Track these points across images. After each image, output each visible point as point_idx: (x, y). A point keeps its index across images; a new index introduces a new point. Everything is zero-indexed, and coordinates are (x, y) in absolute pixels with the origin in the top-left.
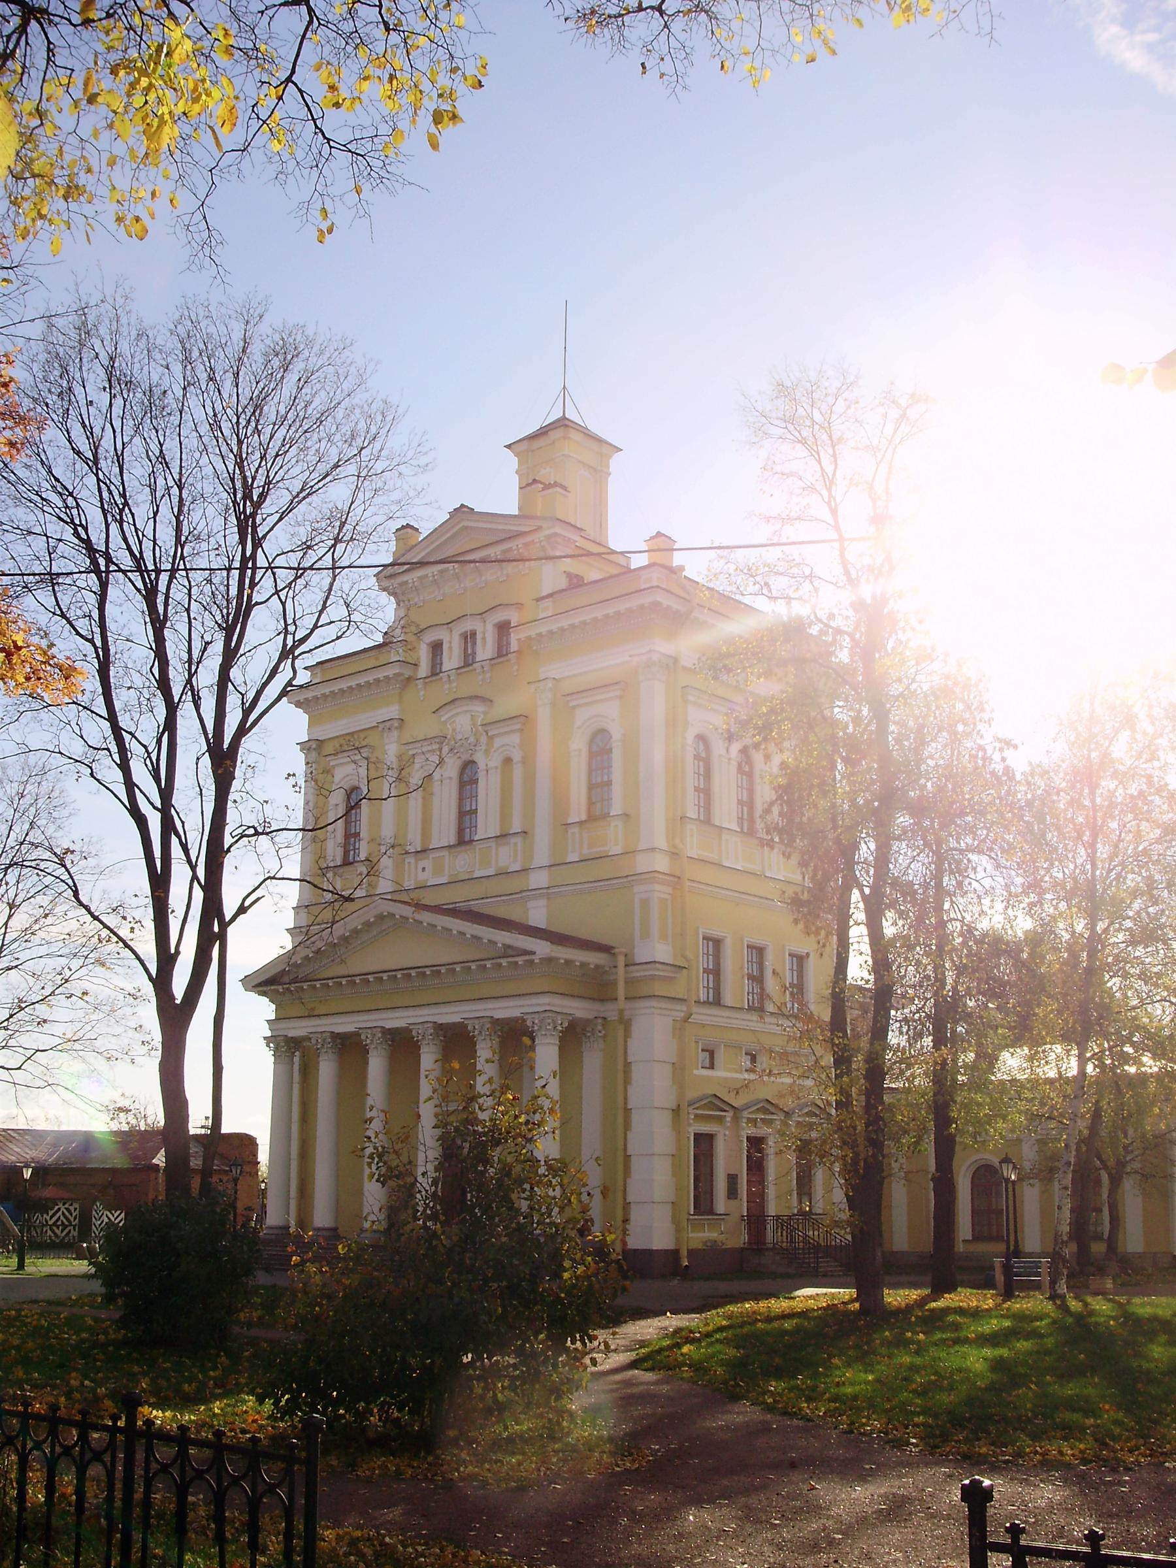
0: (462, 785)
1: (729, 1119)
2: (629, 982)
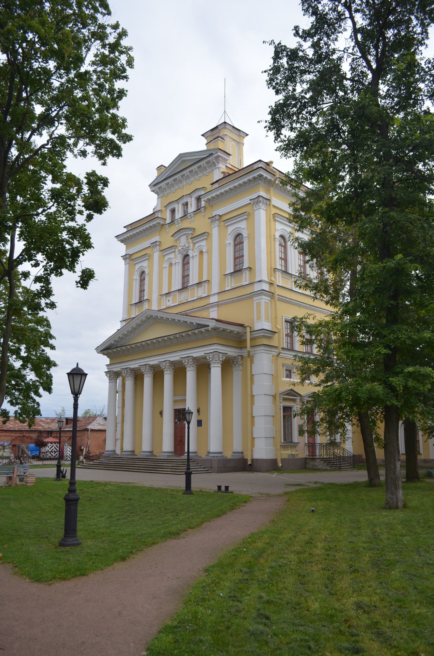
1: (298, 400)
2: (251, 339)
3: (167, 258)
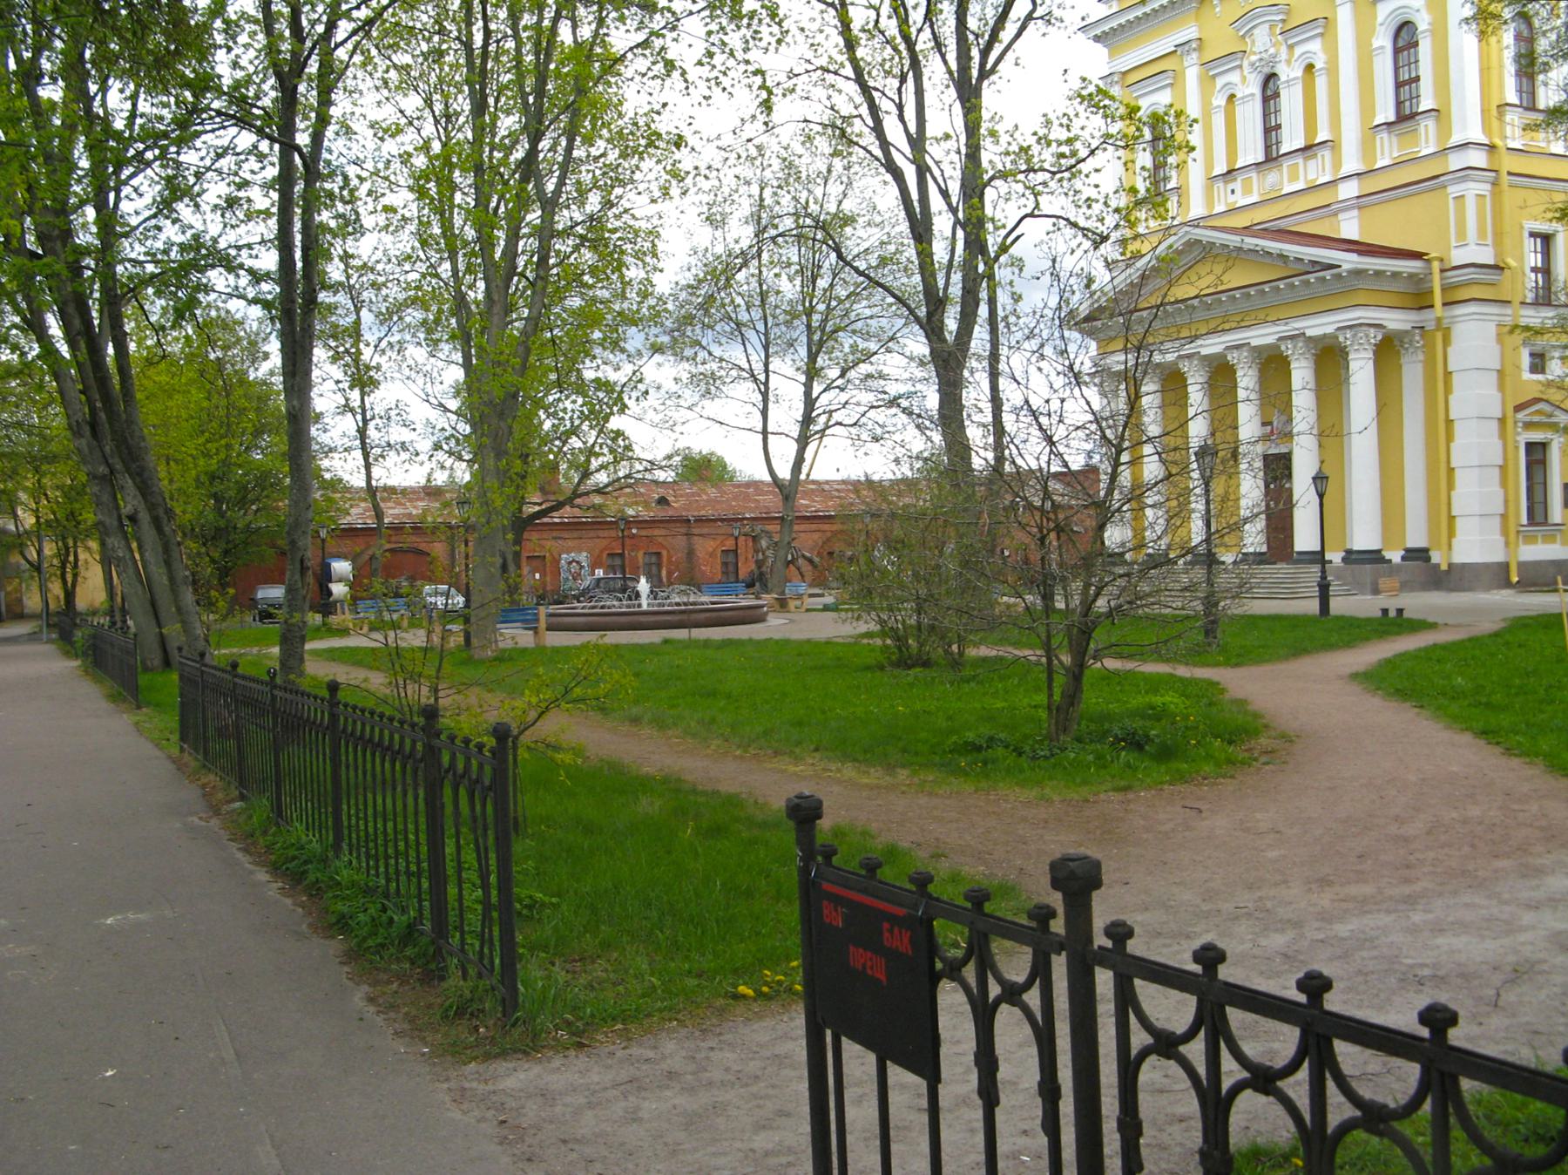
0: (1266, 100)
2: (1444, 289)
3: (1220, 82)
